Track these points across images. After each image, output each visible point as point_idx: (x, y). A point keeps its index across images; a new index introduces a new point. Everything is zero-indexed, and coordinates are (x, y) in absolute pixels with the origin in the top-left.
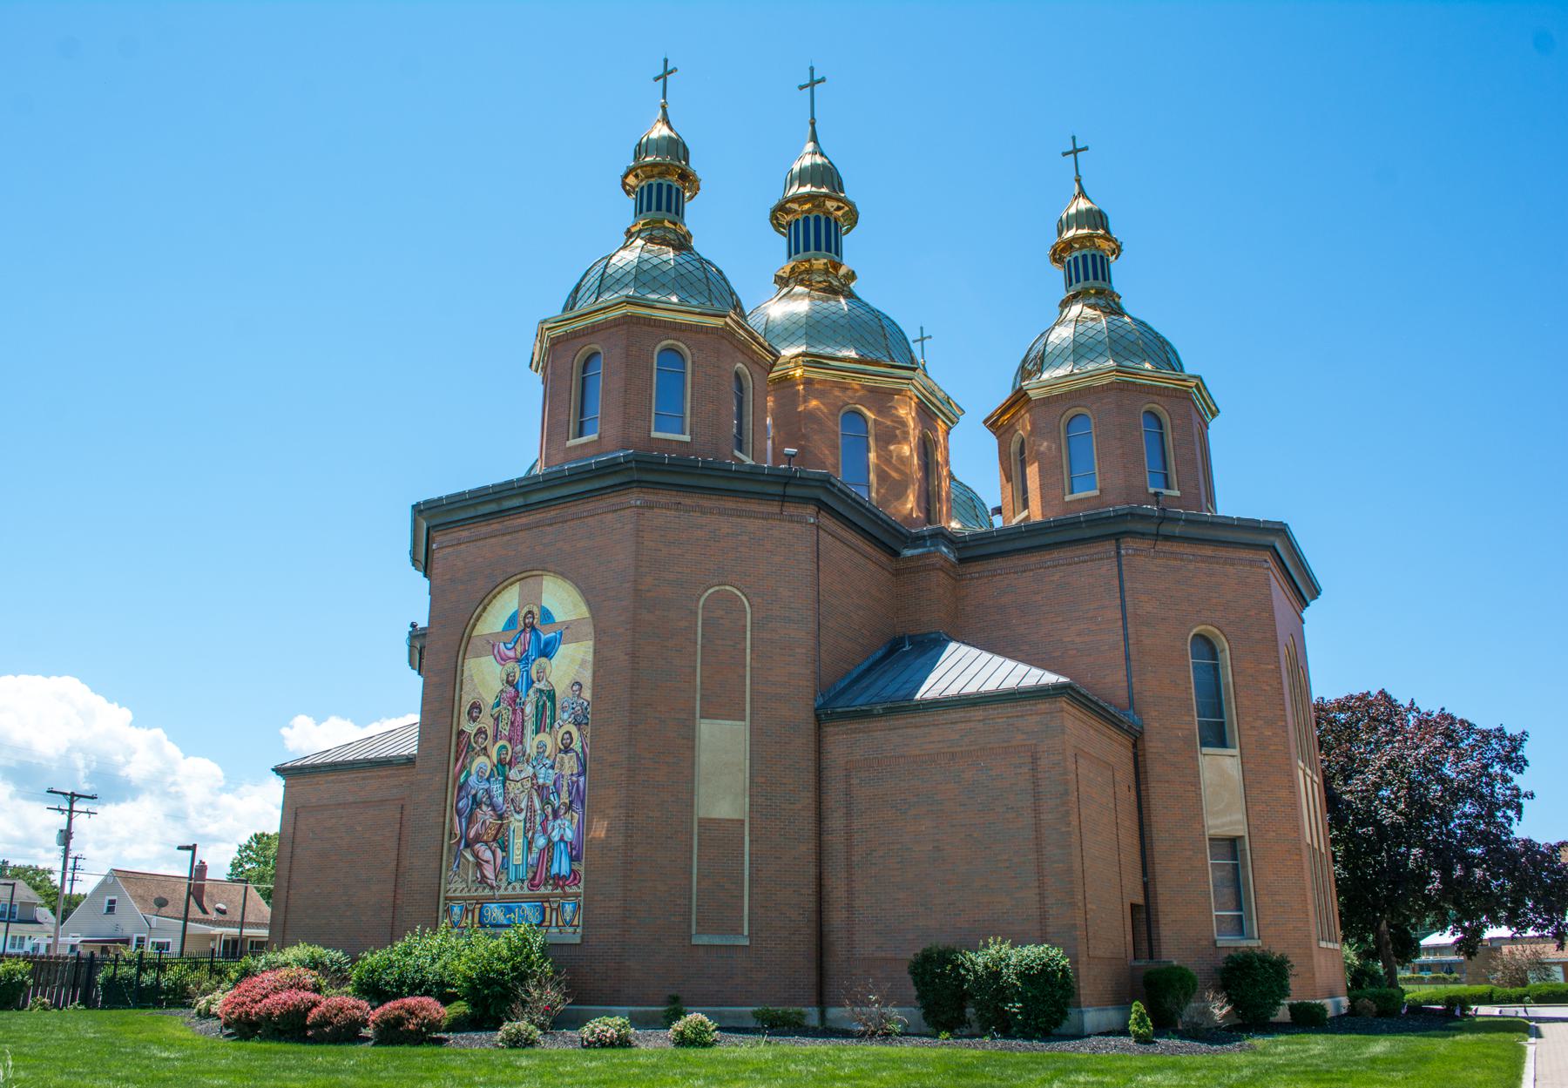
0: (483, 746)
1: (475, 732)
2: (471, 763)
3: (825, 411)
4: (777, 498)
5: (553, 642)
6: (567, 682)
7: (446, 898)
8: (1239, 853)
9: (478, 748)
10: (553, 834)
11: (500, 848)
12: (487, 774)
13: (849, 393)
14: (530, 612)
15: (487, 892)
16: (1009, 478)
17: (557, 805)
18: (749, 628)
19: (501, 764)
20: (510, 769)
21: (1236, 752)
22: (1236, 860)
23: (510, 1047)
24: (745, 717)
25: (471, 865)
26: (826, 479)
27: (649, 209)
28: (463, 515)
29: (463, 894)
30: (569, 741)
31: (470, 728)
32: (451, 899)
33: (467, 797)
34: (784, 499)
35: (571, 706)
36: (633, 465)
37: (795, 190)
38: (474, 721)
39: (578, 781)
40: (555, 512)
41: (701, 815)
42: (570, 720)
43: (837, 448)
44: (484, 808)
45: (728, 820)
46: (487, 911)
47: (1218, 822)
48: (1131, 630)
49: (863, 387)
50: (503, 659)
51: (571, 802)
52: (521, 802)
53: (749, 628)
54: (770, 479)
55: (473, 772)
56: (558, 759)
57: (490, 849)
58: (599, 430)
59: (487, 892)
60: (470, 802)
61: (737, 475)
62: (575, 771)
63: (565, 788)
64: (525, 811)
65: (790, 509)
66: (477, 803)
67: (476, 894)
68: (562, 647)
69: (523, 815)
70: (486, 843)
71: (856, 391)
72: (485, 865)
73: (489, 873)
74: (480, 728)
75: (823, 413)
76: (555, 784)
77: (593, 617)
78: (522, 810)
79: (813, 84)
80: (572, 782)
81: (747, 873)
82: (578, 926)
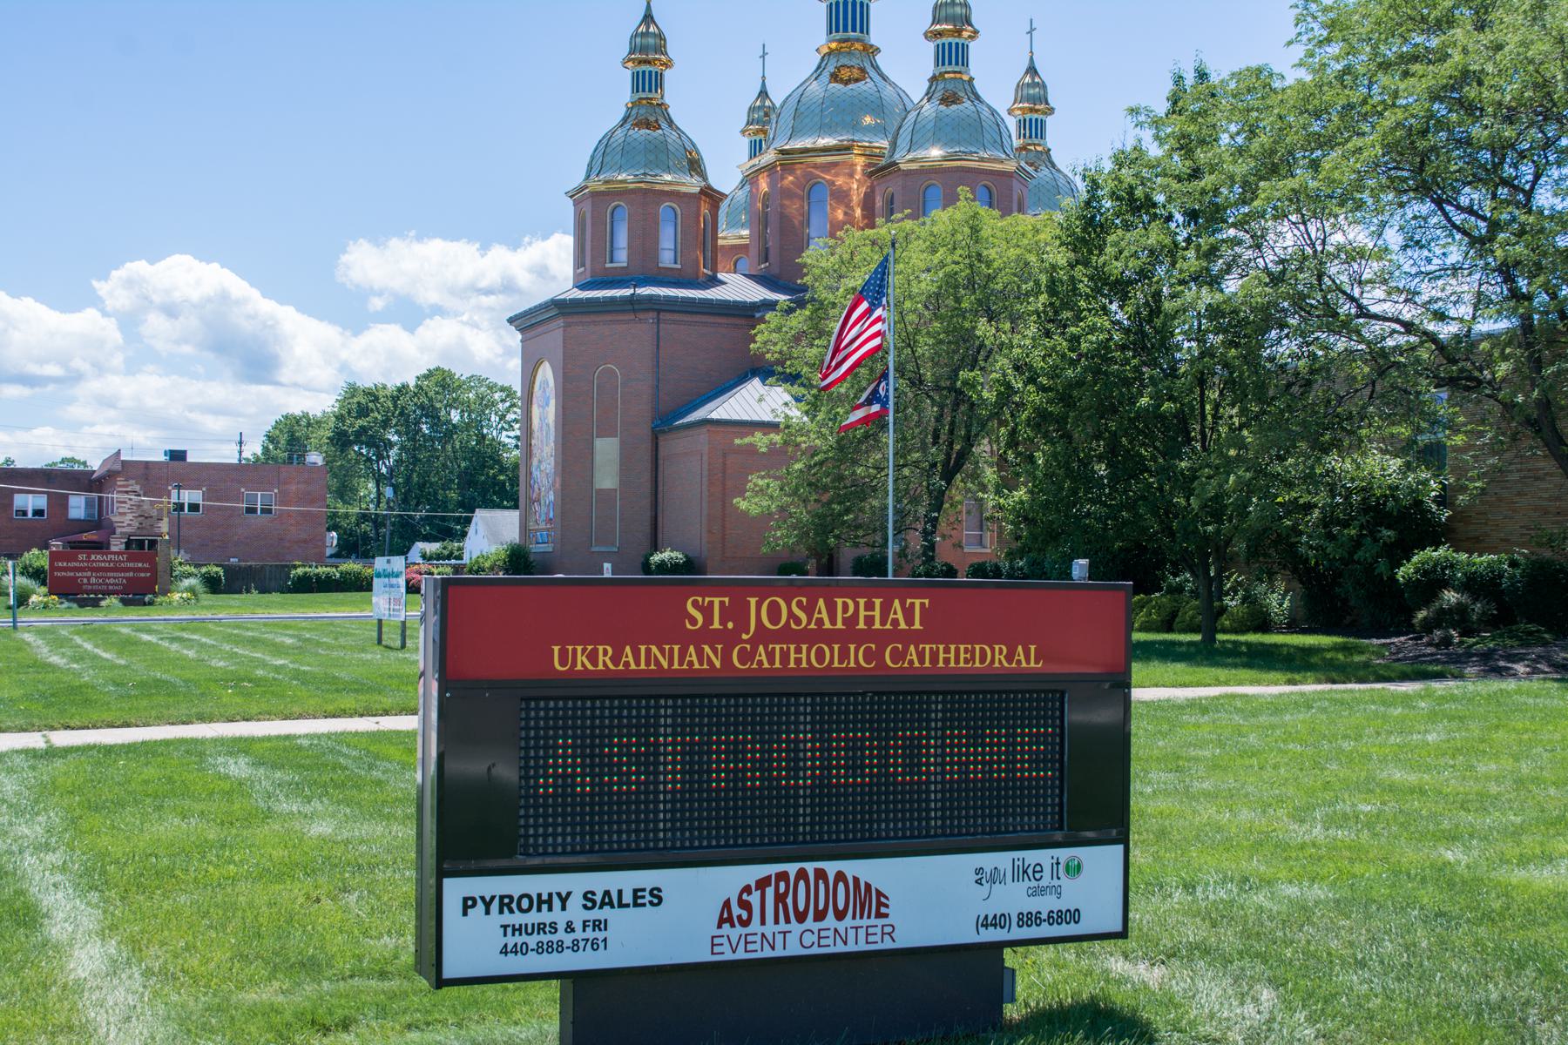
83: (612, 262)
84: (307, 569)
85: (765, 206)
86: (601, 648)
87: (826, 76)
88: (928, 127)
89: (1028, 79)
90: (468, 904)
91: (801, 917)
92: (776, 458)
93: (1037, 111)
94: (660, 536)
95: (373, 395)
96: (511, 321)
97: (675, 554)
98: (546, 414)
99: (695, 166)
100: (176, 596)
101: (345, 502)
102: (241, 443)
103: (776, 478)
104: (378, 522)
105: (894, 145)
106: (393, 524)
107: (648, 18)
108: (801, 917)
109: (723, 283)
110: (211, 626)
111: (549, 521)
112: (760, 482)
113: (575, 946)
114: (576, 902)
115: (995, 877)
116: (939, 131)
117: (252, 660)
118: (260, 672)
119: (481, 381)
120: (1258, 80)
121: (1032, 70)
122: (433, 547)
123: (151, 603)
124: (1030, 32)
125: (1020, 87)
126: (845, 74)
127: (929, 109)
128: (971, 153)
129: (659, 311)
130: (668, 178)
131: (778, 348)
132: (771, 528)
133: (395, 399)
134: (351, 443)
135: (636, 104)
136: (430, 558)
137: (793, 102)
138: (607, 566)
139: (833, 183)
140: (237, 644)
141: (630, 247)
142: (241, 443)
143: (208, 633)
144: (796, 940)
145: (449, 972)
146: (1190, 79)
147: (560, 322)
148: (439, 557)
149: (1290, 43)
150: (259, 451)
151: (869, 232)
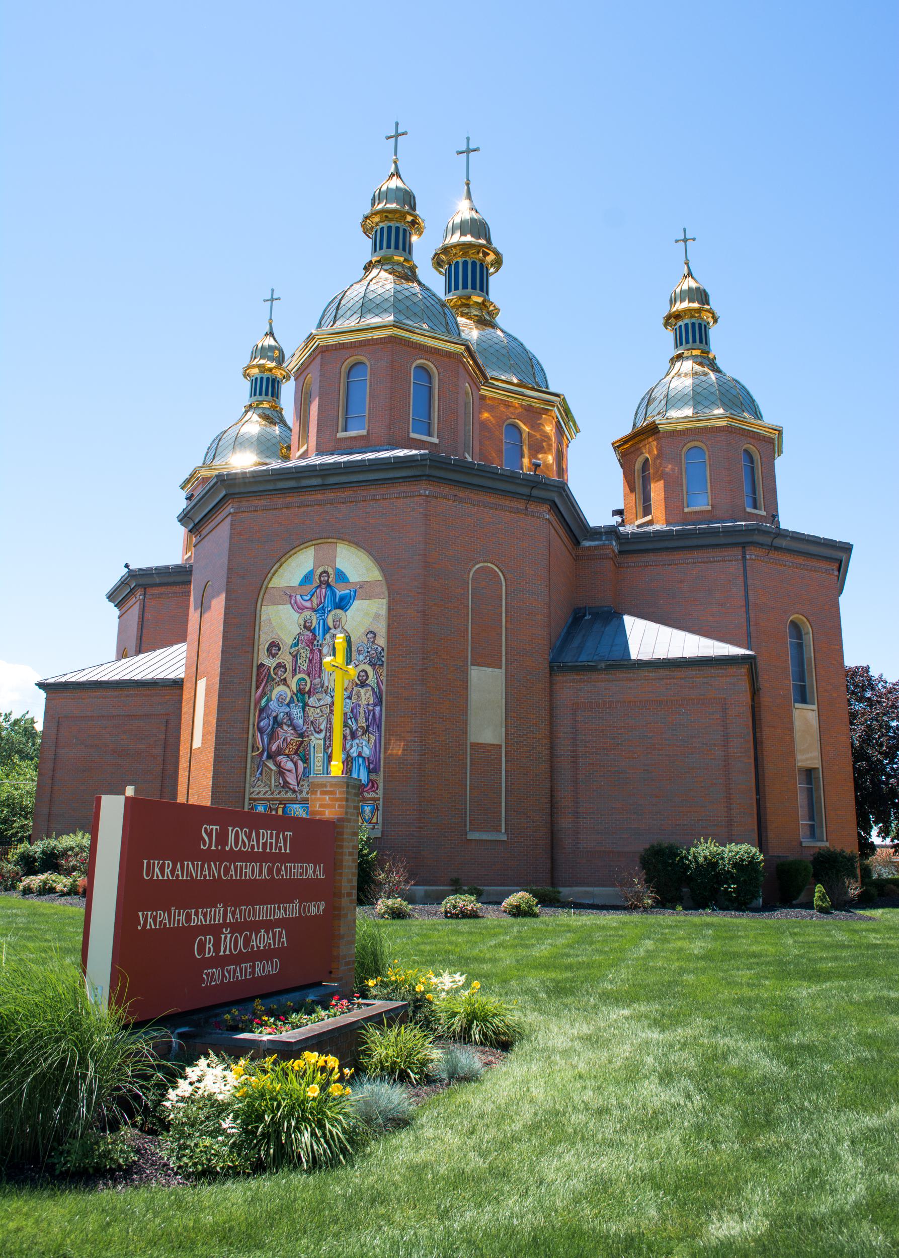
0: (282, 678)
1: (274, 665)
2: (271, 691)
3: (494, 422)
4: (525, 498)
5: (348, 598)
6: (362, 630)
7: (250, 799)
8: (813, 780)
9: (278, 679)
10: (352, 751)
11: (302, 760)
12: (288, 700)
13: (511, 409)
14: (325, 572)
15: (290, 795)
16: (632, 488)
17: (354, 728)
18: (504, 597)
19: (301, 693)
20: (309, 697)
21: (815, 707)
22: (811, 784)
23: (394, 918)
24: (501, 665)
25: (273, 773)
26: (561, 486)
27: (381, 248)
28: (255, 489)
29: (267, 796)
30: (365, 678)
31: (271, 663)
32: (255, 800)
33: (268, 718)
34: (529, 498)
35: (366, 650)
36: (428, 462)
37: (456, 238)
38: (273, 657)
39: (374, 710)
40: (349, 493)
41: (473, 741)
42: (365, 661)
43: (502, 453)
44: (285, 727)
45: (491, 745)
46: (290, 810)
47: (804, 757)
48: (752, 615)
49: (521, 406)
50: (300, 609)
51: (368, 726)
52: (320, 725)
53: (504, 597)
54: (524, 482)
55: (273, 698)
56: (354, 692)
57: (292, 760)
58: (367, 427)
59: (290, 795)
60: (271, 722)
61: (478, 473)
62: (371, 702)
63: (362, 715)
64: (324, 732)
65: (532, 507)
66: (277, 723)
67: (278, 796)
68: (356, 602)
69: (322, 735)
70: (288, 756)
71: (516, 408)
72: (288, 773)
73: (291, 779)
74: (279, 663)
75: (492, 424)
76: (352, 711)
77: (386, 580)
78: (321, 731)
79: (397, 135)
80: (369, 711)
81: (504, 785)
82: (377, 823)
86: (166, 862)
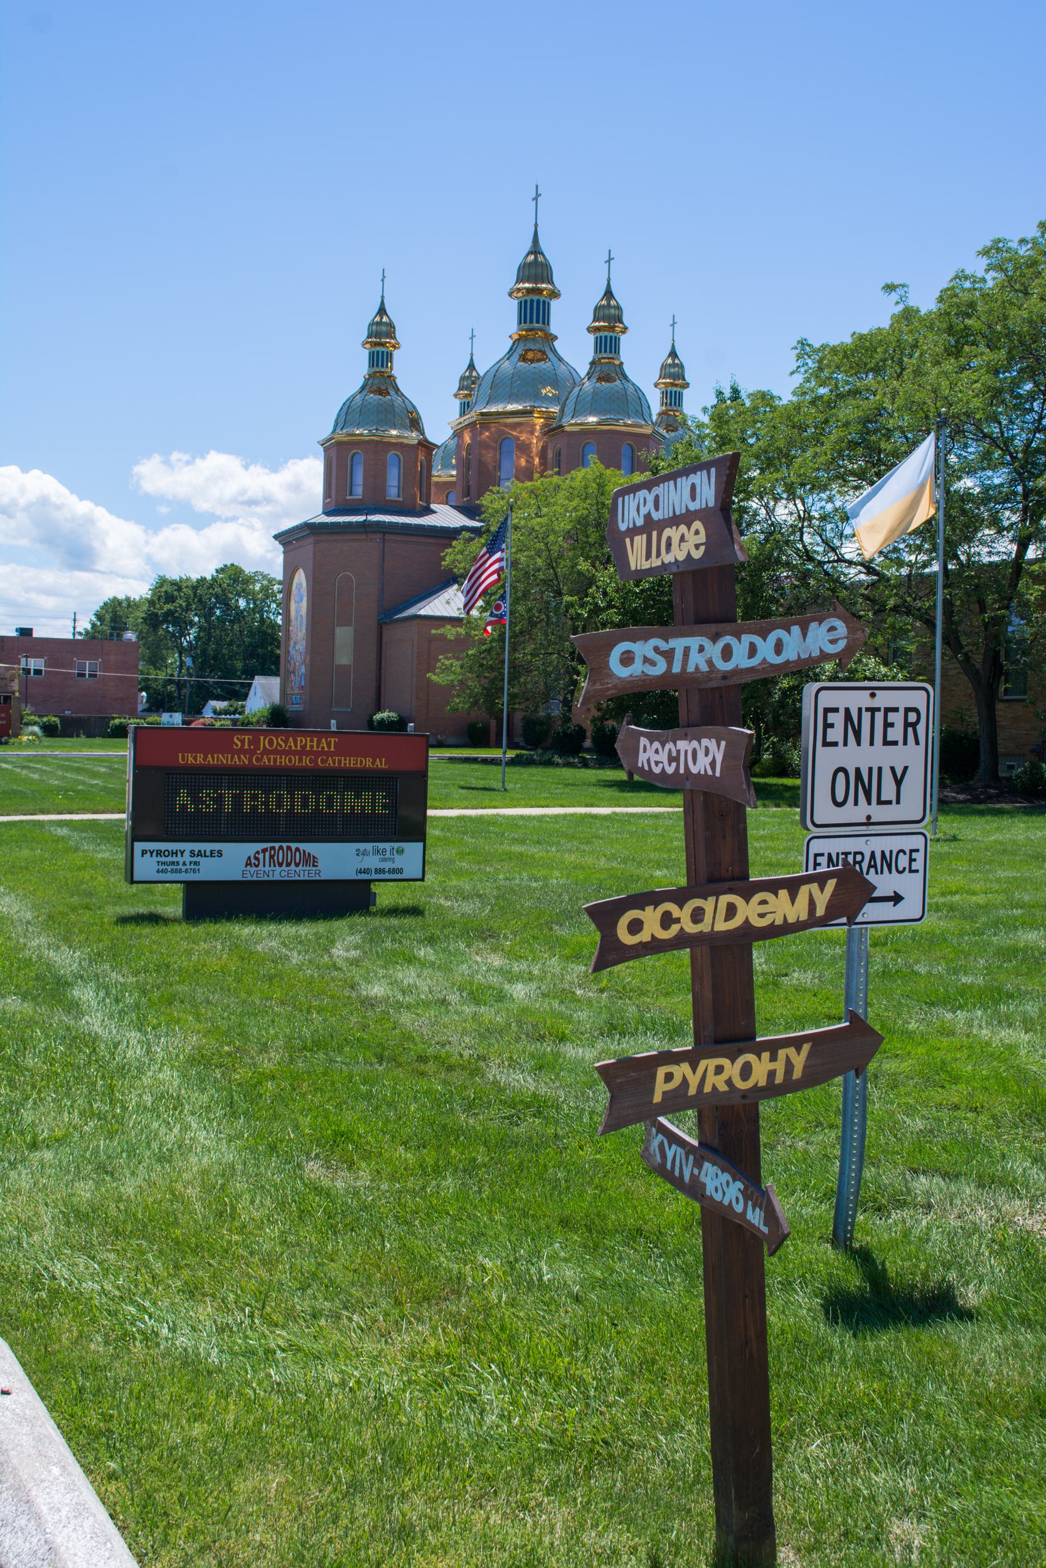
83: (351, 494)
84: (123, 720)
85: (468, 454)
87: (516, 356)
88: (587, 399)
89: (670, 361)
90: (144, 852)
91: (280, 865)
92: (462, 643)
93: (676, 385)
94: (382, 700)
95: (178, 585)
96: (276, 537)
97: (391, 714)
98: (300, 607)
99: (415, 423)
100: (25, 738)
101: (156, 668)
102: (75, 620)
103: (458, 659)
104: (180, 685)
105: (562, 411)
106: (192, 686)
107: (382, 311)
108: (280, 865)
109: (434, 512)
110: (50, 760)
111: (302, 688)
112: (447, 662)
113: (187, 871)
114: (187, 854)
115: (365, 853)
116: (595, 404)
117: (76, 781)
118: (80, 787)
119: (264, 577)
120: (765, 397)
121: (673, 354)
122: (221, 705)
123: (6, 743)
124: (673, 325)
125: (664, 367)
126: (530, 355)
127: (588, 385)
128: (618, 420)
129: (384, 533)
130: (394, 432)
131: (463, 565)
132: (454, 696)
133: (195, 588)
134: (162, 623)
135: (371, 376)
136: (220, 713)
137: (490, 377)
138: (333, 722)
139: (518, 438)
140: (67, 771)
141: (364, 484)
142: (75, 620)
143: (48, 764)
144: (278, 874)
145: (135, 879)
146: (727, 393)
147: (311, 540)
148: (226, 712)
149: (792, 373)
150: (89, 627)
151: (528, 484)
